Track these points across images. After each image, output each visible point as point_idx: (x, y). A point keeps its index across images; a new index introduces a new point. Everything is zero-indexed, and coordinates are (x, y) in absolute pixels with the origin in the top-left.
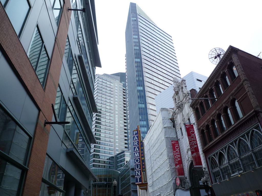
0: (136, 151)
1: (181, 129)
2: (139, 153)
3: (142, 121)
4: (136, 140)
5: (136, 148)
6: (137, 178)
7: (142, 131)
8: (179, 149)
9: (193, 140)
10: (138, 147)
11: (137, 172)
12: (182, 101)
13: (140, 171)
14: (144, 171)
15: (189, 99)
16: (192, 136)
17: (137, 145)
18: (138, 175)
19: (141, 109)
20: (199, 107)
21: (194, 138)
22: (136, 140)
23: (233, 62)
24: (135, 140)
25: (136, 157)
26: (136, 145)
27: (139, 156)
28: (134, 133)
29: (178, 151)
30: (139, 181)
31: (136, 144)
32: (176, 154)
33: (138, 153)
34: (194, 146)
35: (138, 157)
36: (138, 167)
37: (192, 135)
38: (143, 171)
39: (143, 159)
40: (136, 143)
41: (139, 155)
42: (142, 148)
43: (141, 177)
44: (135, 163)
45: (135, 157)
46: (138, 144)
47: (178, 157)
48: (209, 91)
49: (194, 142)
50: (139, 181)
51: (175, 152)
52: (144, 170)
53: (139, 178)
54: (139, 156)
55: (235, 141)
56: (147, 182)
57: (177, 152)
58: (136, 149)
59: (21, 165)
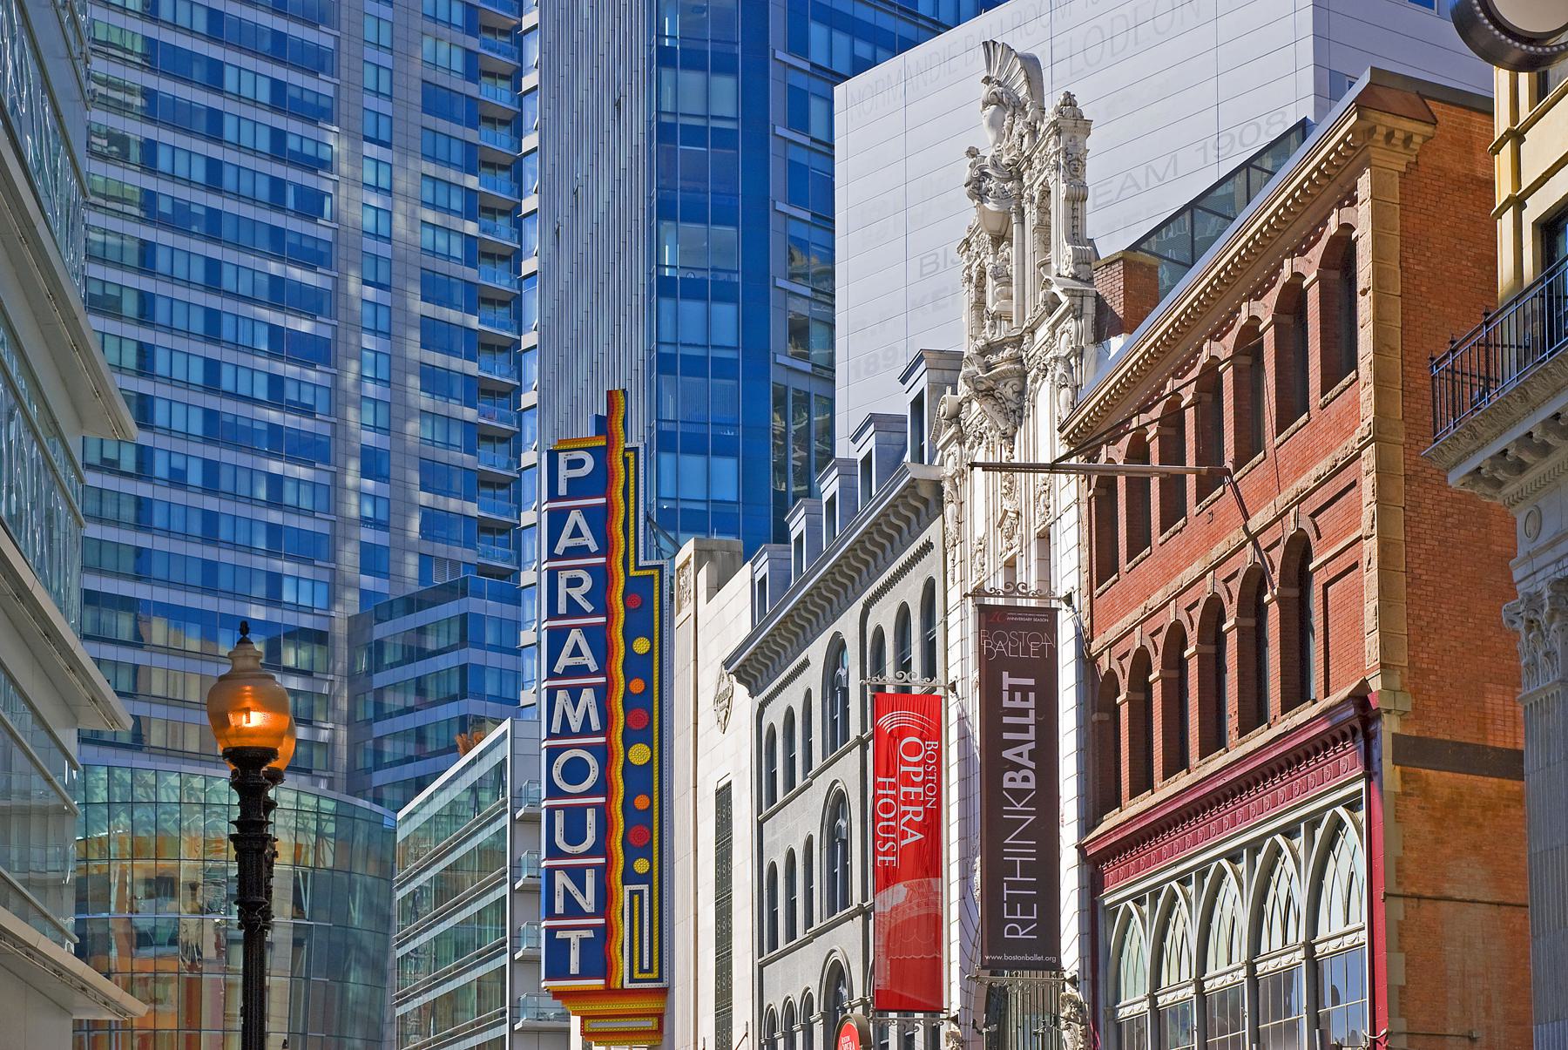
0: (570, 672)
1: (1044, 537)
4: (583, 551)
6: (559, 935)
10: (599, 640)
11: (561, 879)
13: (603, 873)
14: (646, 878)
16: (903, 769)
17: (588, 607)
19: (695, 135)
20: (1316, 288)
21: (914, 784)
22: (583, 551)
23: (1357, 237)
24: (570, 553)
25: (566, 730)
26: (574, 609)
27: (595, 724)
28: (564, 473)
29: (917, 774)
30: (574, 968)
31: (577, 594)
32: (891, 796)
33: (587, 696)
34: (904, 835)
35: (586, 730)
39: (639, 754)
40: (574, 583)
42: (641, 646)
44: (554, 851)
45: (556, 728)
46: (600, 596)
47: (909, 824)
50: (574, 968)
51: (892, 786)
52: (641, 866)
54: (595, 724)
56: (660, 979)
57: (907, 780)
58: (576, 652)
59: (731, 1042)
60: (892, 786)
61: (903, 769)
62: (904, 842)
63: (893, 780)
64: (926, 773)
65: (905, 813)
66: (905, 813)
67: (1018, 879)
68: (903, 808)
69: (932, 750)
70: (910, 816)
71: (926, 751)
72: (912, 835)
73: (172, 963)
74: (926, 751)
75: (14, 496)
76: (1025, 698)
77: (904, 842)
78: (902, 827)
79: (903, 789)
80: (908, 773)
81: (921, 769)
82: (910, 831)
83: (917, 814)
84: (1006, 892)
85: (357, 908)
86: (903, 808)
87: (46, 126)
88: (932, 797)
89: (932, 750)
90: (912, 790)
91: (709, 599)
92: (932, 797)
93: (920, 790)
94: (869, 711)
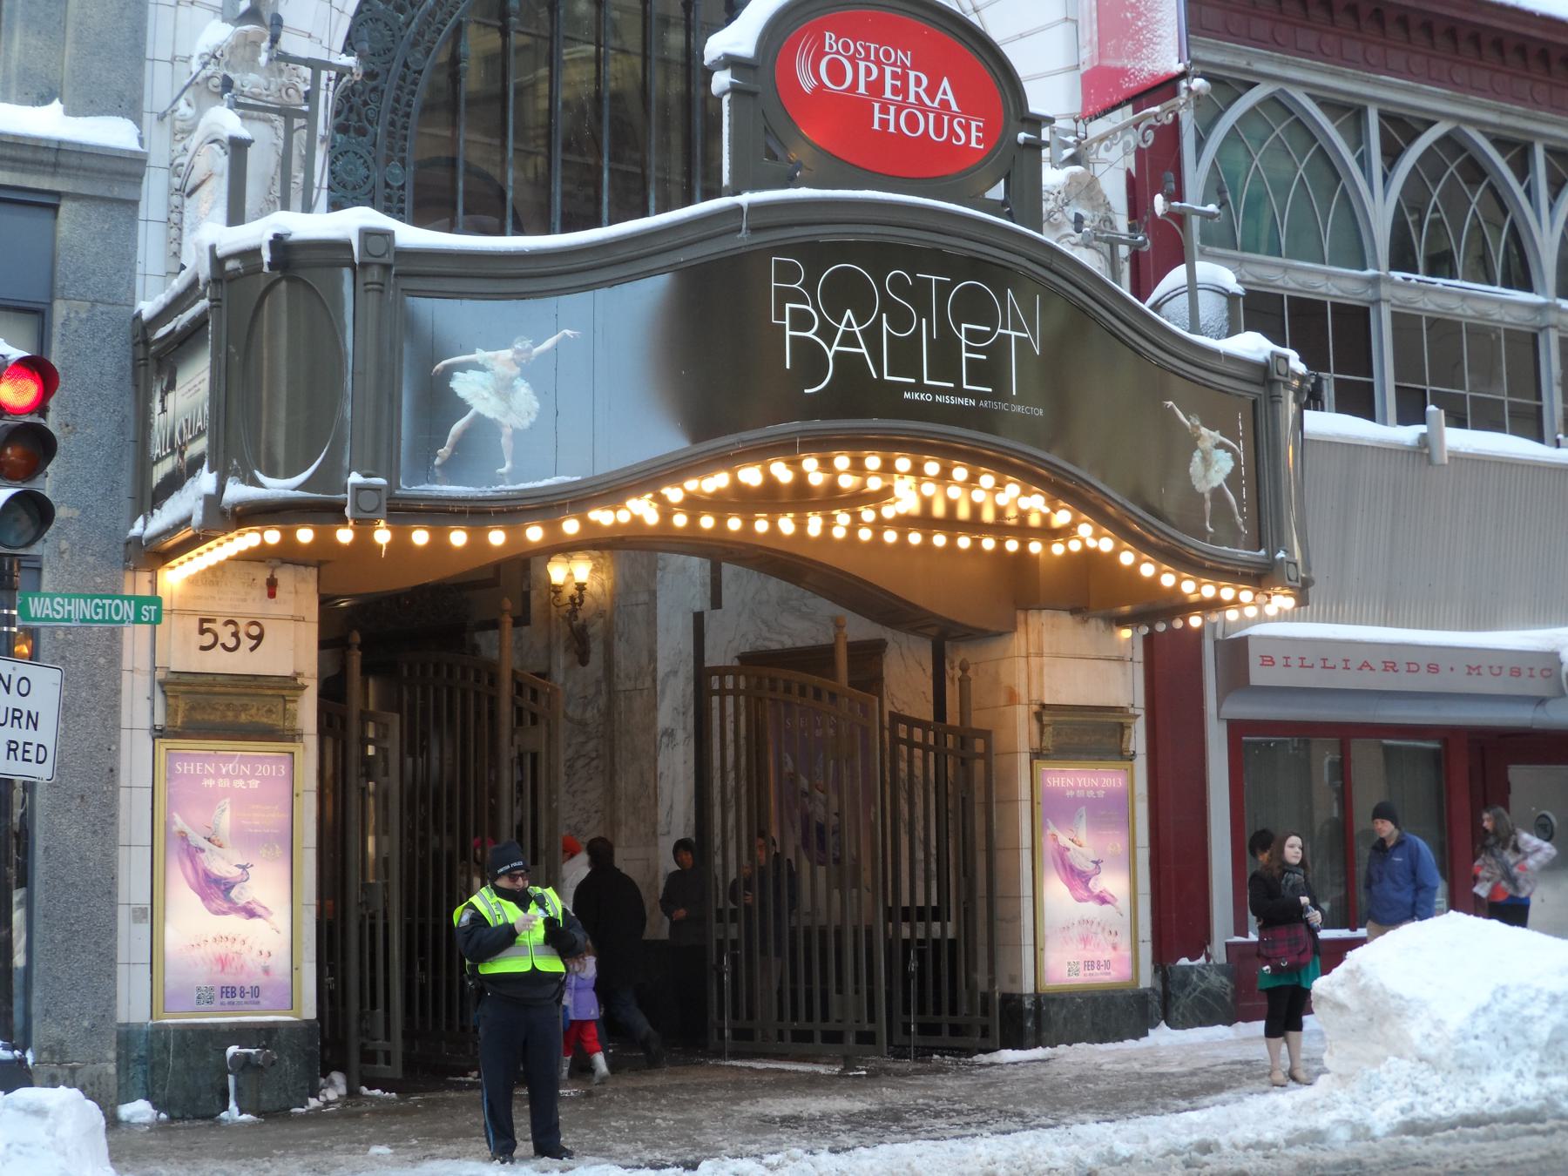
9: (895, 90)
16: (862, 89)
29: (868, 72)
34: (945, 104)
51: (884, 110)
57: (876, 87)
60: (884, 110)
61: (862, 89)
62: (954, 107)
63: (877, 106)
64: (867, 58)
66: (917, 95)
67: (934, 278)
68: (912, 99)
69: (837, 42)
71: (838, 52)
72: (945, 93)
73: (351, 155)
74: (838, 52)
75: (903, 774)
77: (954, 107)
79: (888, 94)
80: (868, 85)
81: (862, 65)
82: (940, 96)
83: (918, 82)
84: (773, 284)
85: (191, 399)
86: (912, 99)
87: (1011, 456)
88: (896, 54)
89: (837, 42)
90: (888, 82)
91: (1508, 812)
92: (896, 54)
93: (888, 70)
94: (880, 851)
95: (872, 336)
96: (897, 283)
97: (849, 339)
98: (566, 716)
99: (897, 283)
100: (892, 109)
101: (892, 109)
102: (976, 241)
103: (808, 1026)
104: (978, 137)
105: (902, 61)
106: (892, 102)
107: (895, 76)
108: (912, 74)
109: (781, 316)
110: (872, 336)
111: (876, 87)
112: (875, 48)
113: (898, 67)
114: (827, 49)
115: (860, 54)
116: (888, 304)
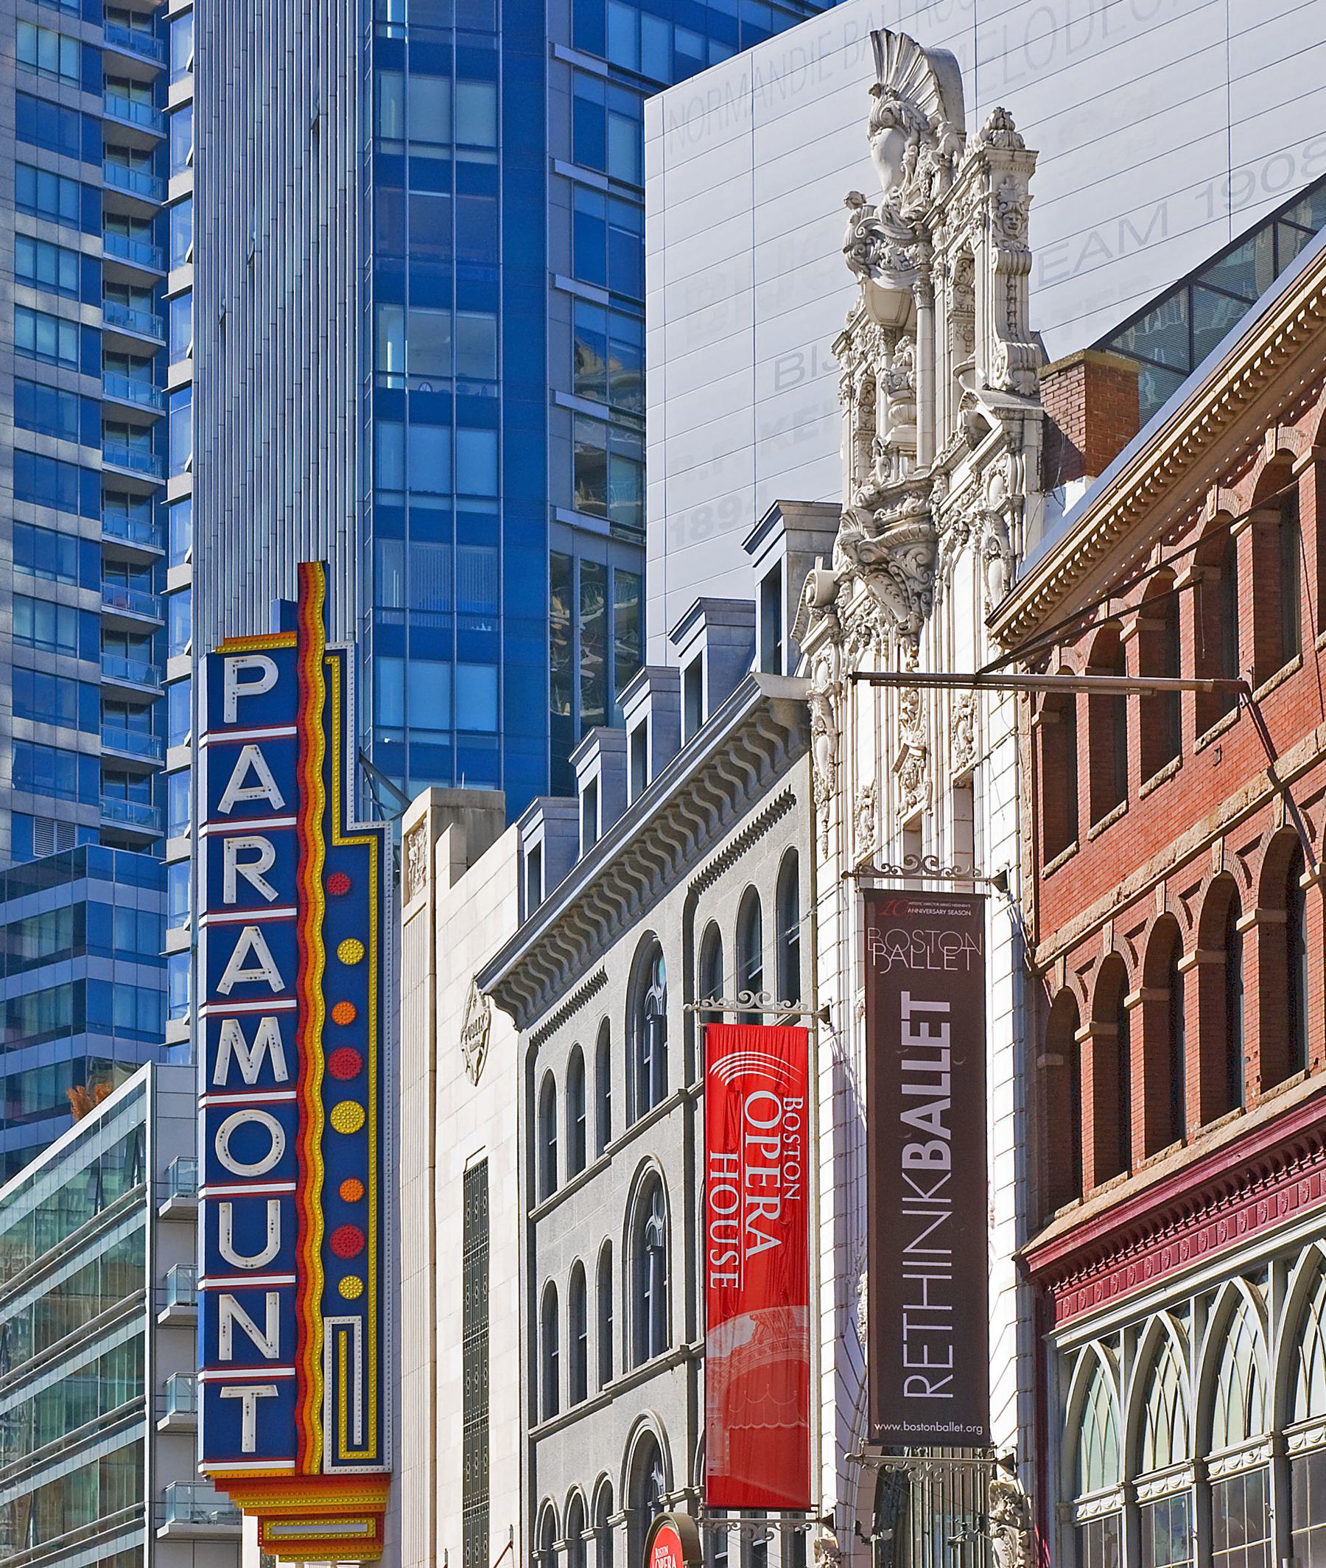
1: (965, 787)
2: (292, 1025)
3: (420, 68)
4: (260, 808)
5: (250, 936)
7: (464, 137)
8: (716, 1189)
9: (754, 1178)
11: (228, 1307)
12: (929, 483)
13: (292, 1299)
14: (358, 1306)
15: (856, 677)
16: (750, 1139)
17: (270, 893)
18: (246, 1353)
22: (260, 808)
24: (242, 810)
25: (235, 1081)
26: (248, 896)
27: (280, 1072)
28: (232, 689)
29: (770, 1148)
30: (248, 1444)
33: (268, 1028)
34: (751, 1240)
35: (266, 1079)
36: (262, 1246)
37: (758, 1132)
38: (332, 1304)
40: (249, 856)
41: (297, 1061)
42: (350, 952)
43: (296, 1390)
48: (1093, 633)
49: (756, 1199)
50: (248, 1444)
51: (733, 1166)
53: (261, 1402)
54: (280, 1072)
55: (1285, 1258)
56: (379, 1460)
57: (755, 1156)
60: (733, 1166)
61: (750, 1139)
62: (750, 1252)
63: (734, 1157)
64: (784, 1146)
65: (753, 1207)
66: (753, 1207)
68: (749, 1199)
70: (760, 1211)
71: (785, 1112)
72: (764, 1241)
74: (785, 1112)
76: (935, 1032)
77: (750, 1252)
78: (748, 1229)
79: (750, 1171)
80: (757, 1145)
81: (777, 1140)
82: (759, 1234)
83: (770, 1208)
86: (749, 1199)
88: (794, 1182)
92: (794, 1182)
93: (776, 1171)
95: (907, 955)
96: (917, 935)
97: (898, 954)
98: (554, 173)
99: (917, 935)
100: (735, 1175)
101: (735, 1175)
102: (318, 1541)
103: (934, 1042)
104: (721, 1280)
105: (789, 1189)
106: (742, 1175)
107: (771, 1178)
108: (776, 1200)
109: (872, 947)
110: (907, 955)
111: (755, 1156)
112: (796, 1156)
113: (781, 1184)
114: (785, 1100)
115: (788, 1138)
116: (913, 942)
